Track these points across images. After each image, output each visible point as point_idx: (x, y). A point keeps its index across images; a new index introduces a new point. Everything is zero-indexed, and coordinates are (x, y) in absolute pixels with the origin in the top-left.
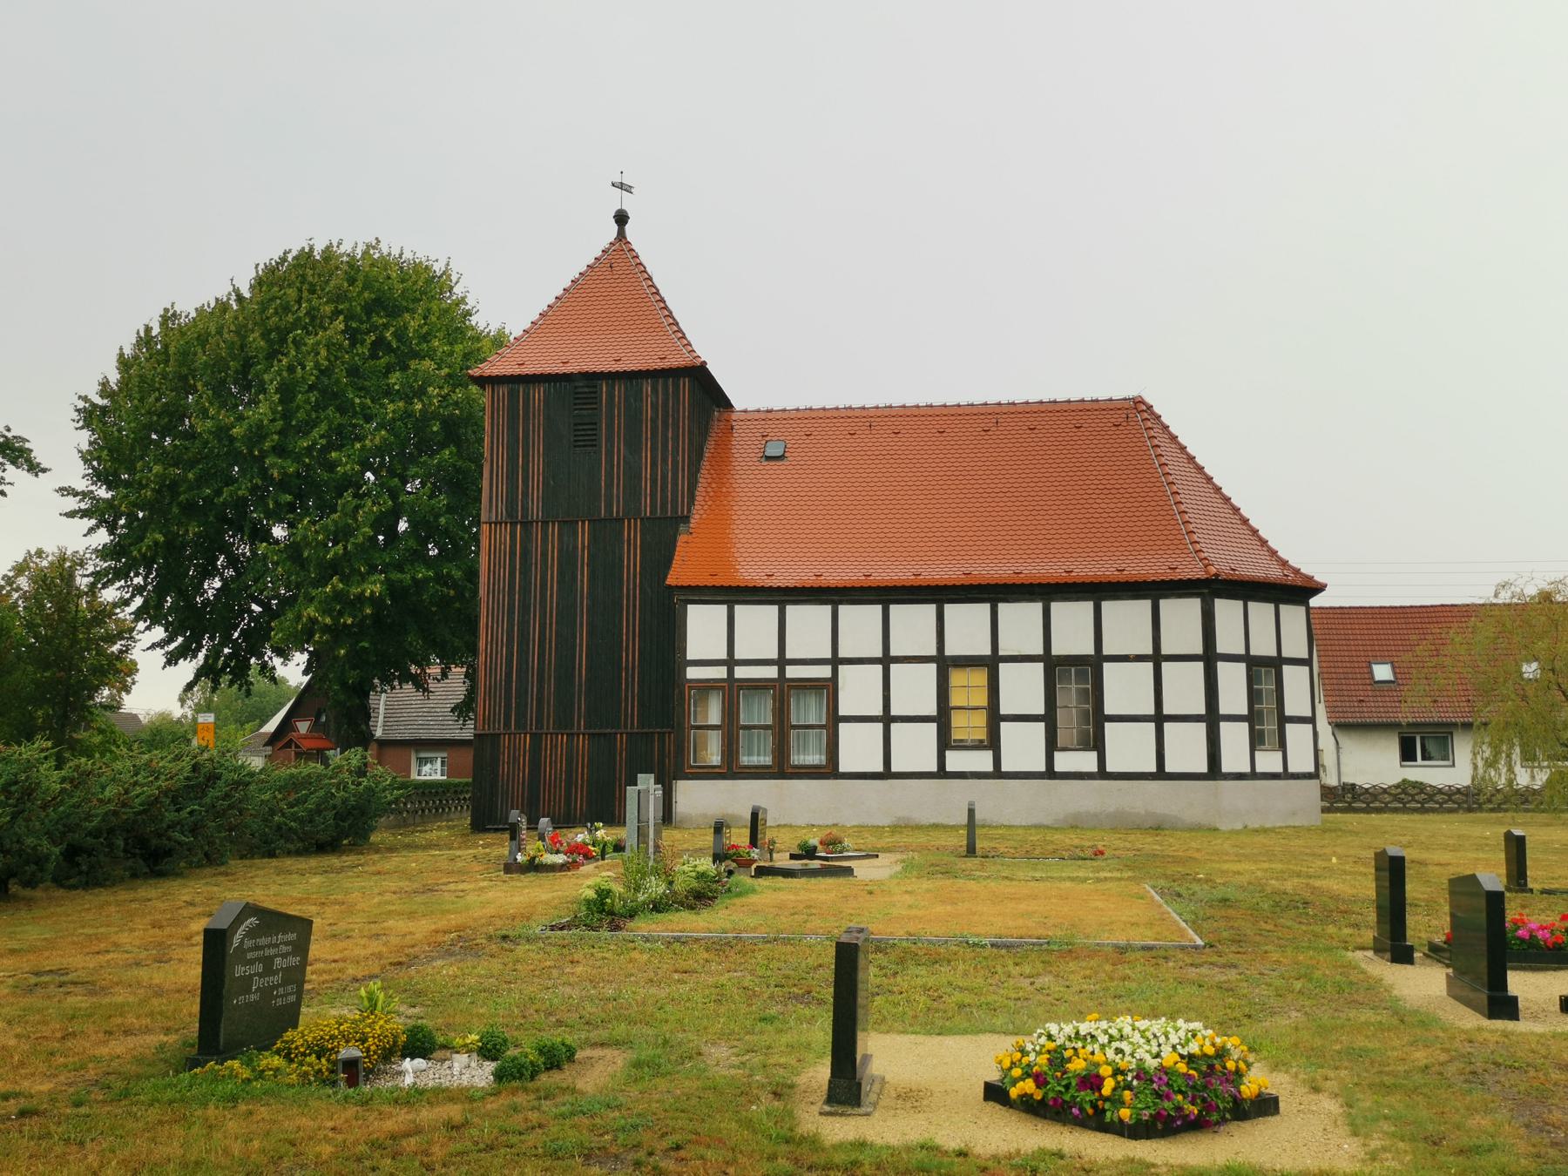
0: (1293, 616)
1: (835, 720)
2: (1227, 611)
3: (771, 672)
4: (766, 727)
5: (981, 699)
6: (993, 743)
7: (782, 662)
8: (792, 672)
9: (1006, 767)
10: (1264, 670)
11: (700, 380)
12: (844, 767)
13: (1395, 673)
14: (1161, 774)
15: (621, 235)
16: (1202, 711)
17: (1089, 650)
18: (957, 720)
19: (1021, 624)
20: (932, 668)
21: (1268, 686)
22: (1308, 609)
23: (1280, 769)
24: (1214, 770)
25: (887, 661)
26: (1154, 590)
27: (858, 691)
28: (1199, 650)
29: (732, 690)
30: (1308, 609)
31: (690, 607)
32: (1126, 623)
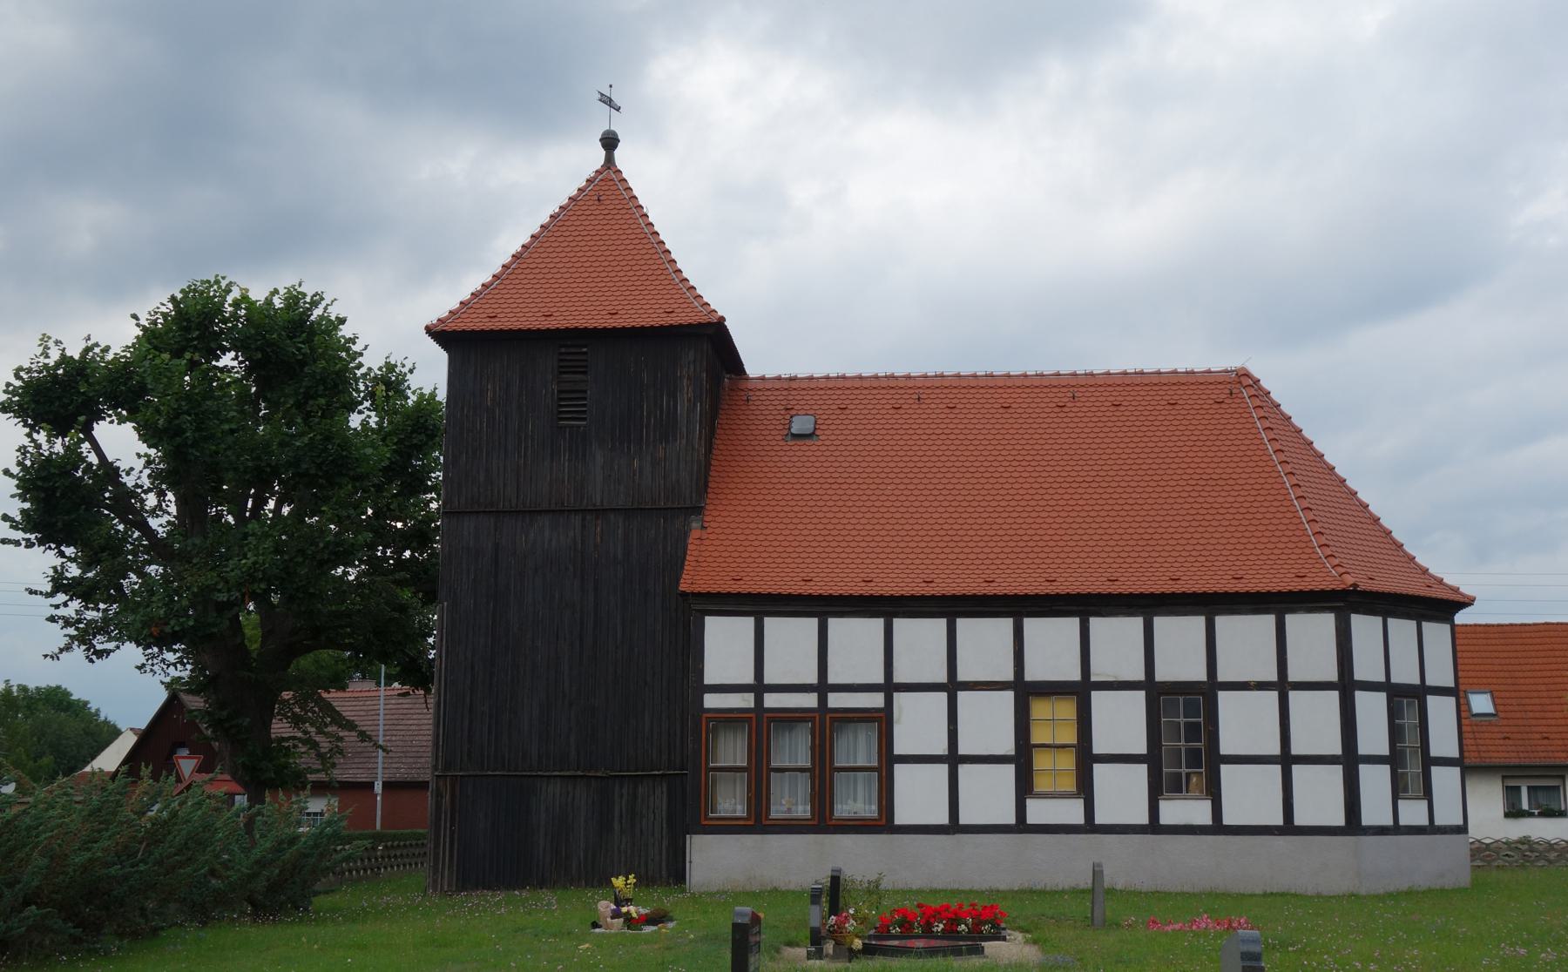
0: (1437, 635)
1: (888, 760)
2: (1365, 628)
3: (809, 701)
4: (802, 770)
5: (1069, 736)
6: (1085, 789)
7: (823, 687)
8: (836, 701)
9: (1228, 819)
10: (1406, 700)
11: (711, 341)
12: (900, 819)
13: (1495, 705)
14: (1288, 828)
15: (610, 160)
16: (1338, 751)
17: (1200, 674)
18: (1041, 761)
19: (1117, 643)
20: (1009, 696)
21: (1410, 720)
22: (1453, 627)
23: (1425, 822)
24: (1353, 824)
25: (952, 687)
26: (1279, 603)
27: (918, 724)
28: (1333, 676)
29: (761, 725)
30: (1453, 627)
31: (708, 619)
32: (1246, 642)
